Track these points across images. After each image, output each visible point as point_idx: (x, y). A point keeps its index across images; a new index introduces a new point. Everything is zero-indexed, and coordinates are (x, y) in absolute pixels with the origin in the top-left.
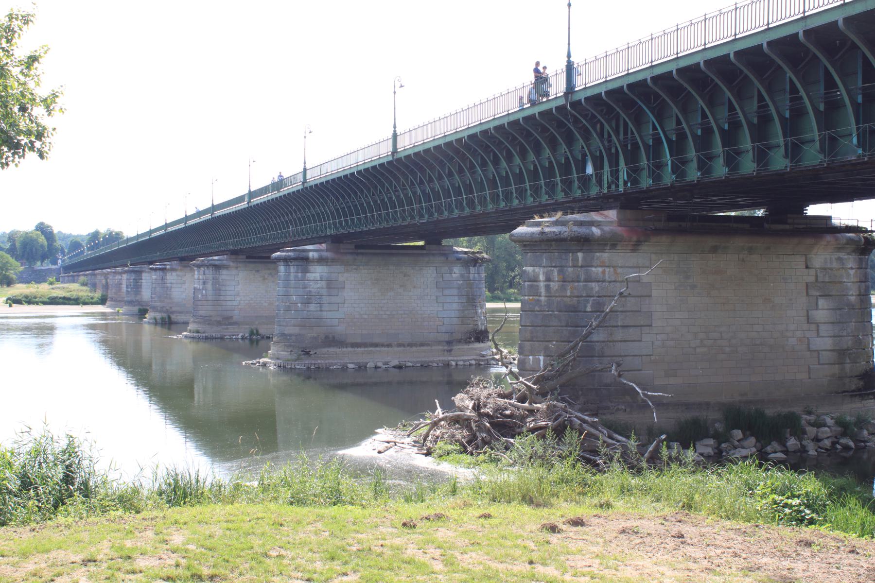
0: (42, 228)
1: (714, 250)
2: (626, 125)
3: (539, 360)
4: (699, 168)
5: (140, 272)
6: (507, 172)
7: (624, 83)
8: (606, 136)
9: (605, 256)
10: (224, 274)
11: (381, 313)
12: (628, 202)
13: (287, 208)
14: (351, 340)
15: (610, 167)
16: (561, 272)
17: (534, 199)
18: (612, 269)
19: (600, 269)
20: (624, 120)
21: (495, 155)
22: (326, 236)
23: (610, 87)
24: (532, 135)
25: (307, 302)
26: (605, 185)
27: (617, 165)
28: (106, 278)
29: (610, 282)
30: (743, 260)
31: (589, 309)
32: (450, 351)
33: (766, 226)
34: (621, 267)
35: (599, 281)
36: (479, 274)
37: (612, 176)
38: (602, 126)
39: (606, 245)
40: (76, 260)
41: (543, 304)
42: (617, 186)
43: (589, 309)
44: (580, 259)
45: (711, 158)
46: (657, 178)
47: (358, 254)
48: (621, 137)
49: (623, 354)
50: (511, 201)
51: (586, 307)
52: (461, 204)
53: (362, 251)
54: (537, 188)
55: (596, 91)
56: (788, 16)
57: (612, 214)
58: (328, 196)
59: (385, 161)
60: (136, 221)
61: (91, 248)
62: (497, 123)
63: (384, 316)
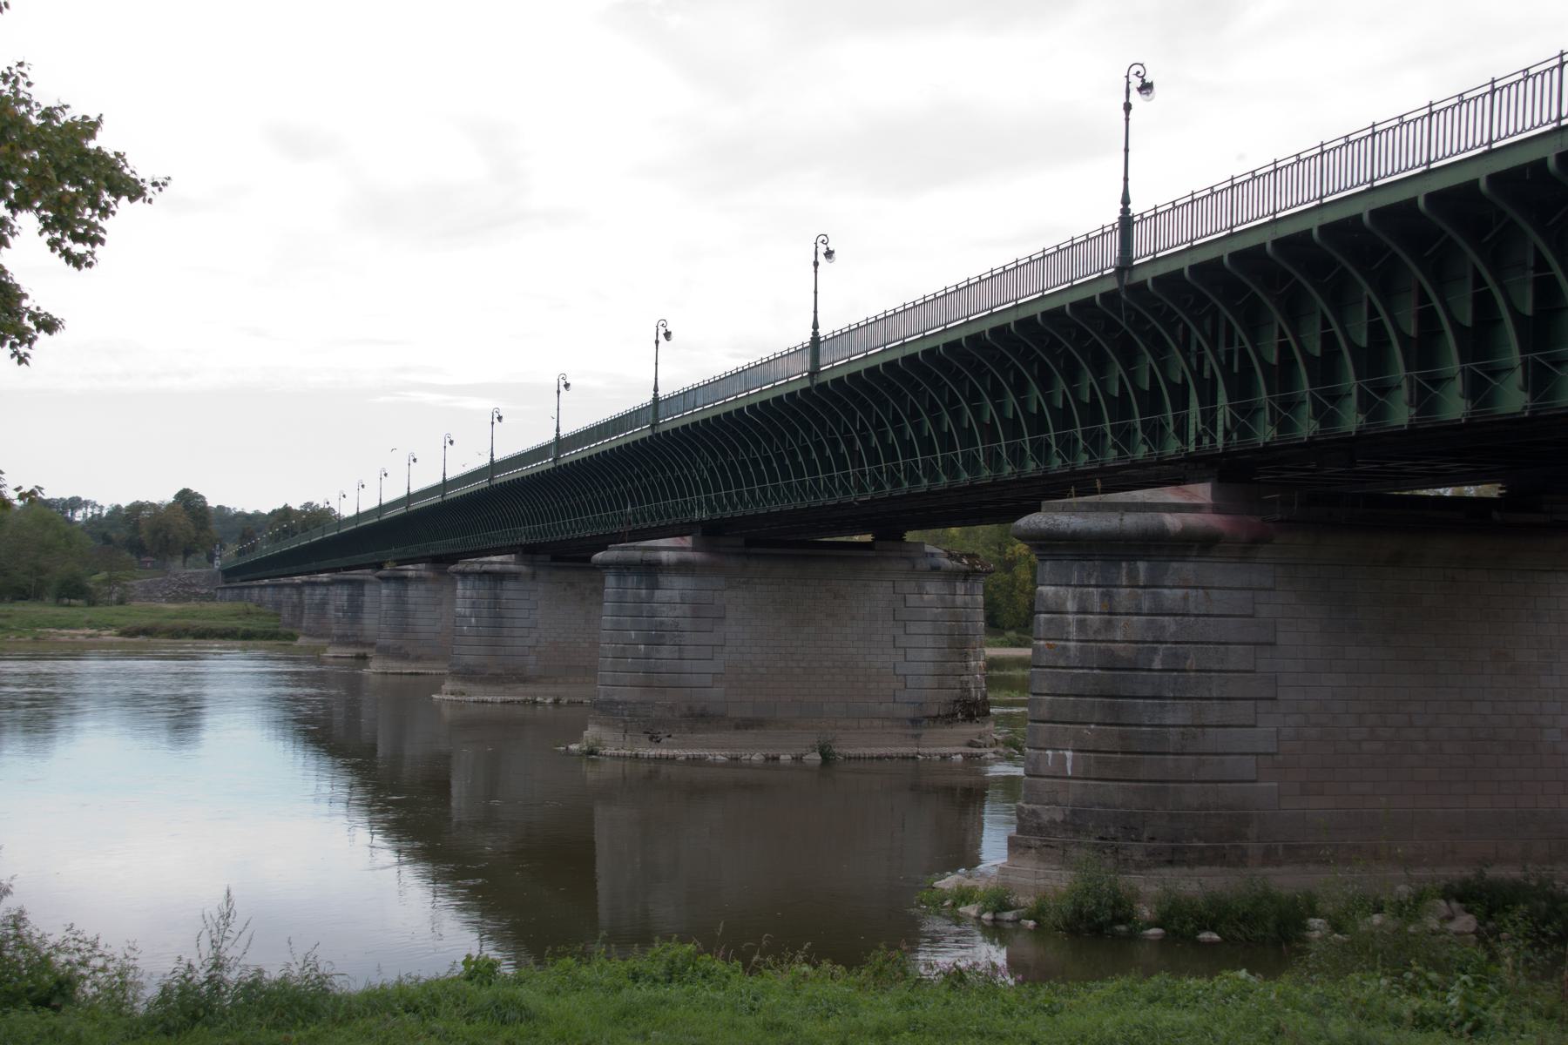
0: (187, 499)
2: (1230, 330)
4: (1316, 416)
5: (361, 584)
6: (1039, 404)
7: (1224, 252)
8: (1194, 348)
9: (1187, 569)
10: (510, 591)
12: (1232, 470)
13: (624, 471)
15: (1201, 404)
16: (1108, 597)
17: (1091, 457)
18: (1201, 591)
19: (1180, 592)
20: (1228, 321)
21: (1020, 376)
22: (691, 523)
23: (1200, 257)
24: (1061, 344)
25: (654, 642)
26: (1192, 437)
27: (1214, 400)
28: (300, 594)
31: (1157, 665)
32: (917, 737)
33: (1496, 515)
36: (971, 599)
37: (1203, 423)
38: (1187, 330)
41: (1072, 653)
42: (1213, 440)
43: (1157, 665)
45: (1437, 382)
46: (1285, 425)
48: (1222, 349)
49: (1220, 750)
50: (1074, 457)
51: (1152, 661)
52: (953, 465)
53: (758, 550)
54: (1128, 431)
55: (1174, 266)
56: (1528, 126)
57: (1202, 492)
58: (697, 451)
59: (798, 387)
60: (355, 486)
61: (276, 538)
62: (996, 322)
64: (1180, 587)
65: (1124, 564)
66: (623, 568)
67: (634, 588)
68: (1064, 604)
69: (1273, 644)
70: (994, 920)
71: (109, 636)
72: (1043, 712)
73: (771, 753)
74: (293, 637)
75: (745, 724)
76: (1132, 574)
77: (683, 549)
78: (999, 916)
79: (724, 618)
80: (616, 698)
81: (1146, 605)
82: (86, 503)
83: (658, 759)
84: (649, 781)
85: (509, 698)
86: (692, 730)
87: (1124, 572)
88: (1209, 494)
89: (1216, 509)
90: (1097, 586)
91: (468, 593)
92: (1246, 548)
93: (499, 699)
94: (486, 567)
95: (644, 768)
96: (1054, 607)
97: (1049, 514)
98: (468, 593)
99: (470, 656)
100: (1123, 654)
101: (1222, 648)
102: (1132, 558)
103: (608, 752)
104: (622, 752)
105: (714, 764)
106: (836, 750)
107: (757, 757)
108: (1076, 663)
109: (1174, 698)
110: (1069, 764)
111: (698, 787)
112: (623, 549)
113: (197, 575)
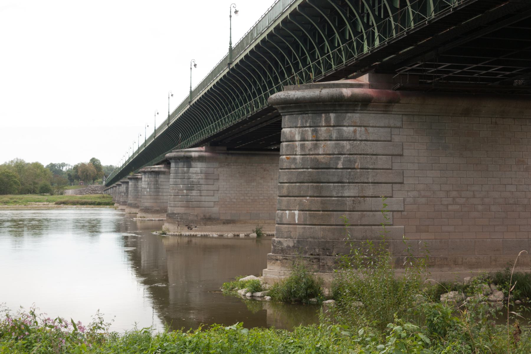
1: (466, 113)
3: (294, 214)
9: (356, 117)
11: (246, 198)
14: (222, 217)
16: (315, 132)
18: (363, 128)
19: (352, 129)
29: (361, 141)
30: (496, 123)
31: (340, 166)
34: (373, 127)
35: (350, 140)
39: (356, 105)
40: (109, 180)
41: (298, 161)
43: (340, 166)
44: (332, 120)
47: (228, 154)
49: (373, 209)
51: (337, 164)
53: (232, 152)
63: (249, 200)
64: (352, 125)
65: (323, 115)
66: (177, 159)
67: (182, 167)
68: (294, 136)
69: (401, 155)
70: (252, 296)
71: (51, 205)
72: (285, 192)
73: (236, 233)
74: (113, 204)
75: (227, 222)
76: (328, 120)
77: (202, 151)
78: (254, 294)
79: (218, 179)
80: (175, 212)
81: (334, 136)
82: (67, 165)
83: (190, 236)
84: (188, 245)
85: (161, 219)
86: (205, 224)
87: (323, 119)
88: (368, 79)
89: (371, 86)
90: (310, 127)
91: (146, 179)
92: (387, 106)
93: (157, 219)
94: (153, 170)
95: (186, 240)
96: (289, 139)
97: (286, 92)
98: (146, 179)
99: (147, 203)
100: (323, 161)
101: (374, 157)
102: (327, 112)
103: (170, 233)
104: (175, 233)
105: (213, 238)
106: (263, 232)
107: (230, 235)
108: (300, 166)
109: (349, 183)
110: (296, 217)
111: (208, 248)
112: (177, 152)
113: (97, 187)
